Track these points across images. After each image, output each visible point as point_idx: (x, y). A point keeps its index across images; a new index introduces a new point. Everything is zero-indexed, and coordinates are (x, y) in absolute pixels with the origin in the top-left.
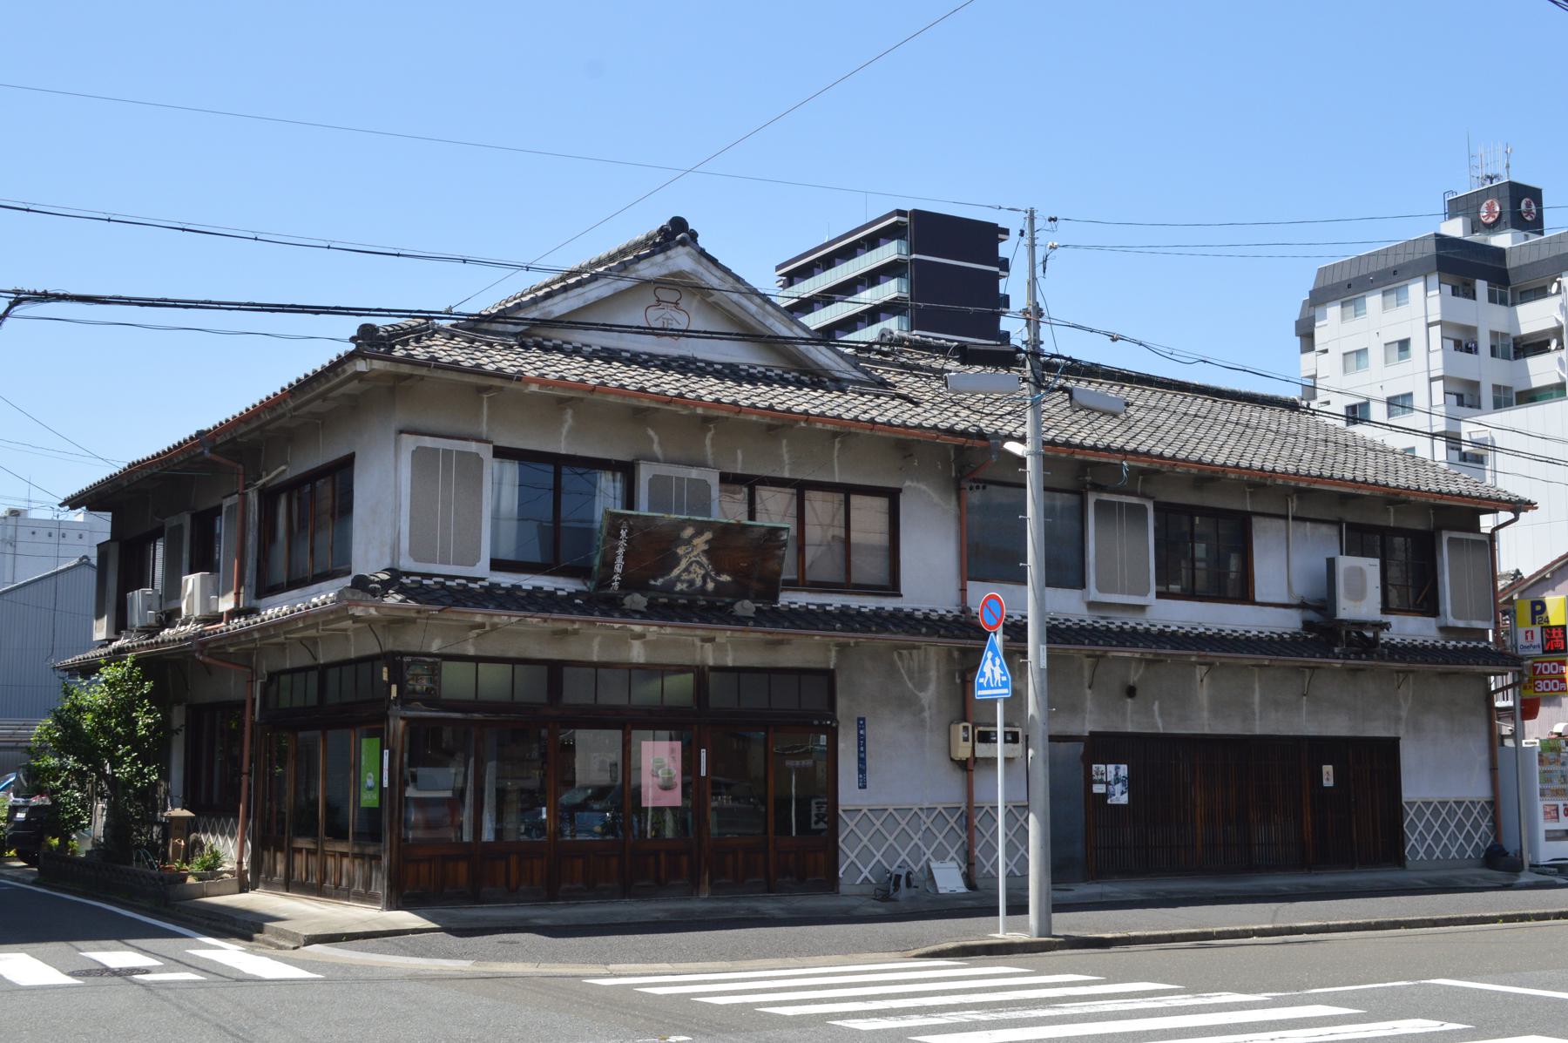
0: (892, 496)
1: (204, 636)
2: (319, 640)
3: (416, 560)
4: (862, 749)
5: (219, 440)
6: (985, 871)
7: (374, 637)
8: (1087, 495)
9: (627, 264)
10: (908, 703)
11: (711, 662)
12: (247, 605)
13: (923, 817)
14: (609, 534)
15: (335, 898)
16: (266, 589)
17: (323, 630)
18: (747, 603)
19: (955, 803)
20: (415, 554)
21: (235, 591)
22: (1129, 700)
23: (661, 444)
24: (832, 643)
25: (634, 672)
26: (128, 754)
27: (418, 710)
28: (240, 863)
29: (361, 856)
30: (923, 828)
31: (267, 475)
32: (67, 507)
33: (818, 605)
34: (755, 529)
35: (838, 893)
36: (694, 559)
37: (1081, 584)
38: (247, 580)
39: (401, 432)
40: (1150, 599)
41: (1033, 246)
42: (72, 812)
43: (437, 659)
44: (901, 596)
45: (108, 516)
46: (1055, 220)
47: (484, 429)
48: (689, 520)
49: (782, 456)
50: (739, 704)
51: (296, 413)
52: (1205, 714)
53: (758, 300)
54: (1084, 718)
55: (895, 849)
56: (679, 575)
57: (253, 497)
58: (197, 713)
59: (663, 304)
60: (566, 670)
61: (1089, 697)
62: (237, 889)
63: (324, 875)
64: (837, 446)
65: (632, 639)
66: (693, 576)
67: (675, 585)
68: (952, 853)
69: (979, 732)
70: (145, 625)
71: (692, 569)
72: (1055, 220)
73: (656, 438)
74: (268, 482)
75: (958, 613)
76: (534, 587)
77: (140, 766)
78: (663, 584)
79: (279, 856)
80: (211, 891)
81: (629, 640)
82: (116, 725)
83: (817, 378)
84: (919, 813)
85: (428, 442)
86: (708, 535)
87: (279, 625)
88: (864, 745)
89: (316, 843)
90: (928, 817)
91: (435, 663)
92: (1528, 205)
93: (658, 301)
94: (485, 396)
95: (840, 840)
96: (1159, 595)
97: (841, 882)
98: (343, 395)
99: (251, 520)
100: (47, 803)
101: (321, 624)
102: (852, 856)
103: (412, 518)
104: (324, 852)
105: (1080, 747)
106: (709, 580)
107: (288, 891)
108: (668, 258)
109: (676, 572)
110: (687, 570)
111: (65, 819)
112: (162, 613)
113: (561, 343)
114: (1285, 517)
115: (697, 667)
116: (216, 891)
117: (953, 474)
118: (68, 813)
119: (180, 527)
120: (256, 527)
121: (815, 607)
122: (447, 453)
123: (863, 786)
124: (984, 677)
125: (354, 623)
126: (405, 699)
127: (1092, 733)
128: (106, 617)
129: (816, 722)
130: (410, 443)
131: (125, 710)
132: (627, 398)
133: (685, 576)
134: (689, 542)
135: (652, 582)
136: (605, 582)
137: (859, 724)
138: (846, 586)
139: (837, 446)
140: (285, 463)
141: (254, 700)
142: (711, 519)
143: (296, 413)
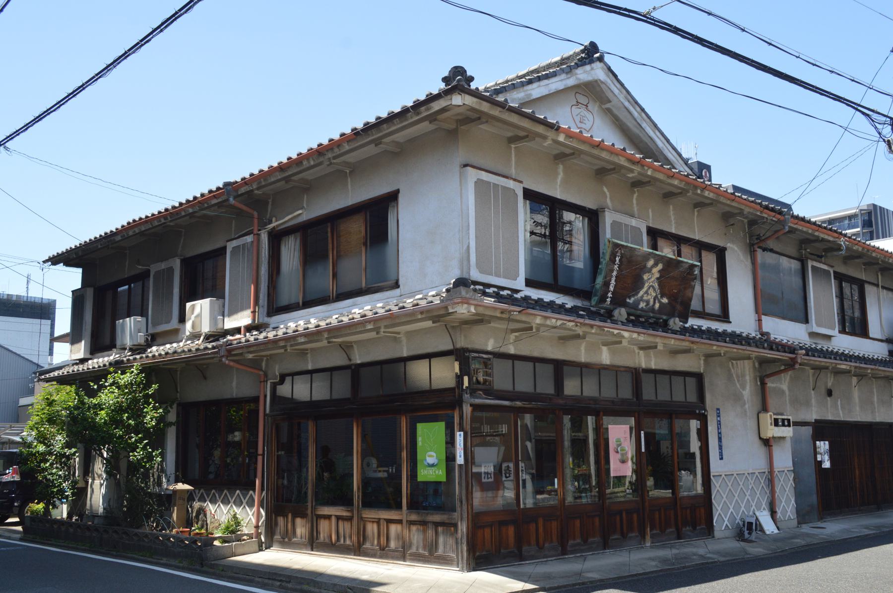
1: (231, 344)
2: (353, 344)
3: (481, 272)
5: (242, 190)
7: (449, 335)
8: (807, 262)
9: (572, 68)
10: (737, 398)
11: (644, 366)
12: (261, 321)
13: (750, 479)
15: (381, 557)
16: (276, 308)
17: (384, 332)
19: (762, 469)
21: (252, 309)
22: (828, 398)
23: (611, 199)
24: (701, 354)
25: (603, 372)
26: (140, 441)
27: (481, 398)
28: (257, 527)
29: (424, 523)
30: (750, 488)
31: (276, 221)
32: (50, 263)
33: (698, 326)
34: (684, 265)
35: (713, 537)
37: (807, 321)
38: (261, 302)
39: (466, 165)
40: (835, 332)
42: (59, 486)
43: (490, 356)
44: (731, 322)
45: (79, 271)
47: (513, 172)
48: (652, 253)
49: (670, 217)
50: (657, 398)
51: (335, 161)
52: (858, 408)
53: (638, 109)
54: (812, 410)
55: (727, 505)
56: (642, 296)
57: (264, 237)
58: (186, 409)
59: (580, 105)
61: (813, 395)
62: (257, 548)
63: (363, 537)
64: (696, 214)
65: (603, 345)
67: (639, 304)
68: (764, 506)
70: (136, 343)
73: (608, 194)
74: (278, 226)
77: (150, 450)
79: (299, 521)
80: (240, 550)
81: (601, 346)
82: (128, 418)
85: (485, 176)
87: (289, 339)
89: (352, 511)
90: (752, 480)
91: (489, 359)
92: (706, 173)
93: (577, 102)
94: (513, 146)
95: (713, 497)
96: (840, 332)
98: (393, 141)
99: (263, 255)
100: (16, 479)
101: (382, 327)
102: (719, 509)
103: (476, 237)
104: (361, 519)
106: (657, 301)
107: (312, 550)
108: (592, 69)
109: (641, 293)
110: (646, 292)
111: (53, 492)
112: (148, 336)
114: (877, 285)
115: (635, 369)
116: (240, 550)
117: (748, 241)
118: (55, 487)
119: (171, 270)
120: (267, 261)
121: (696, 327)
122: (496, 186)
123: (721, 459)
125: (433, 323)
126: (472, 391)
128: (83, 342)
130: (473, 175)
131: (135, 409)
132: (613, 156)
133: (645, 298)
134: (650, 271)
136: (603, 299)
139: (696, 214)
140: (302, 208)
141: (265, 396)
142: (664, 254)
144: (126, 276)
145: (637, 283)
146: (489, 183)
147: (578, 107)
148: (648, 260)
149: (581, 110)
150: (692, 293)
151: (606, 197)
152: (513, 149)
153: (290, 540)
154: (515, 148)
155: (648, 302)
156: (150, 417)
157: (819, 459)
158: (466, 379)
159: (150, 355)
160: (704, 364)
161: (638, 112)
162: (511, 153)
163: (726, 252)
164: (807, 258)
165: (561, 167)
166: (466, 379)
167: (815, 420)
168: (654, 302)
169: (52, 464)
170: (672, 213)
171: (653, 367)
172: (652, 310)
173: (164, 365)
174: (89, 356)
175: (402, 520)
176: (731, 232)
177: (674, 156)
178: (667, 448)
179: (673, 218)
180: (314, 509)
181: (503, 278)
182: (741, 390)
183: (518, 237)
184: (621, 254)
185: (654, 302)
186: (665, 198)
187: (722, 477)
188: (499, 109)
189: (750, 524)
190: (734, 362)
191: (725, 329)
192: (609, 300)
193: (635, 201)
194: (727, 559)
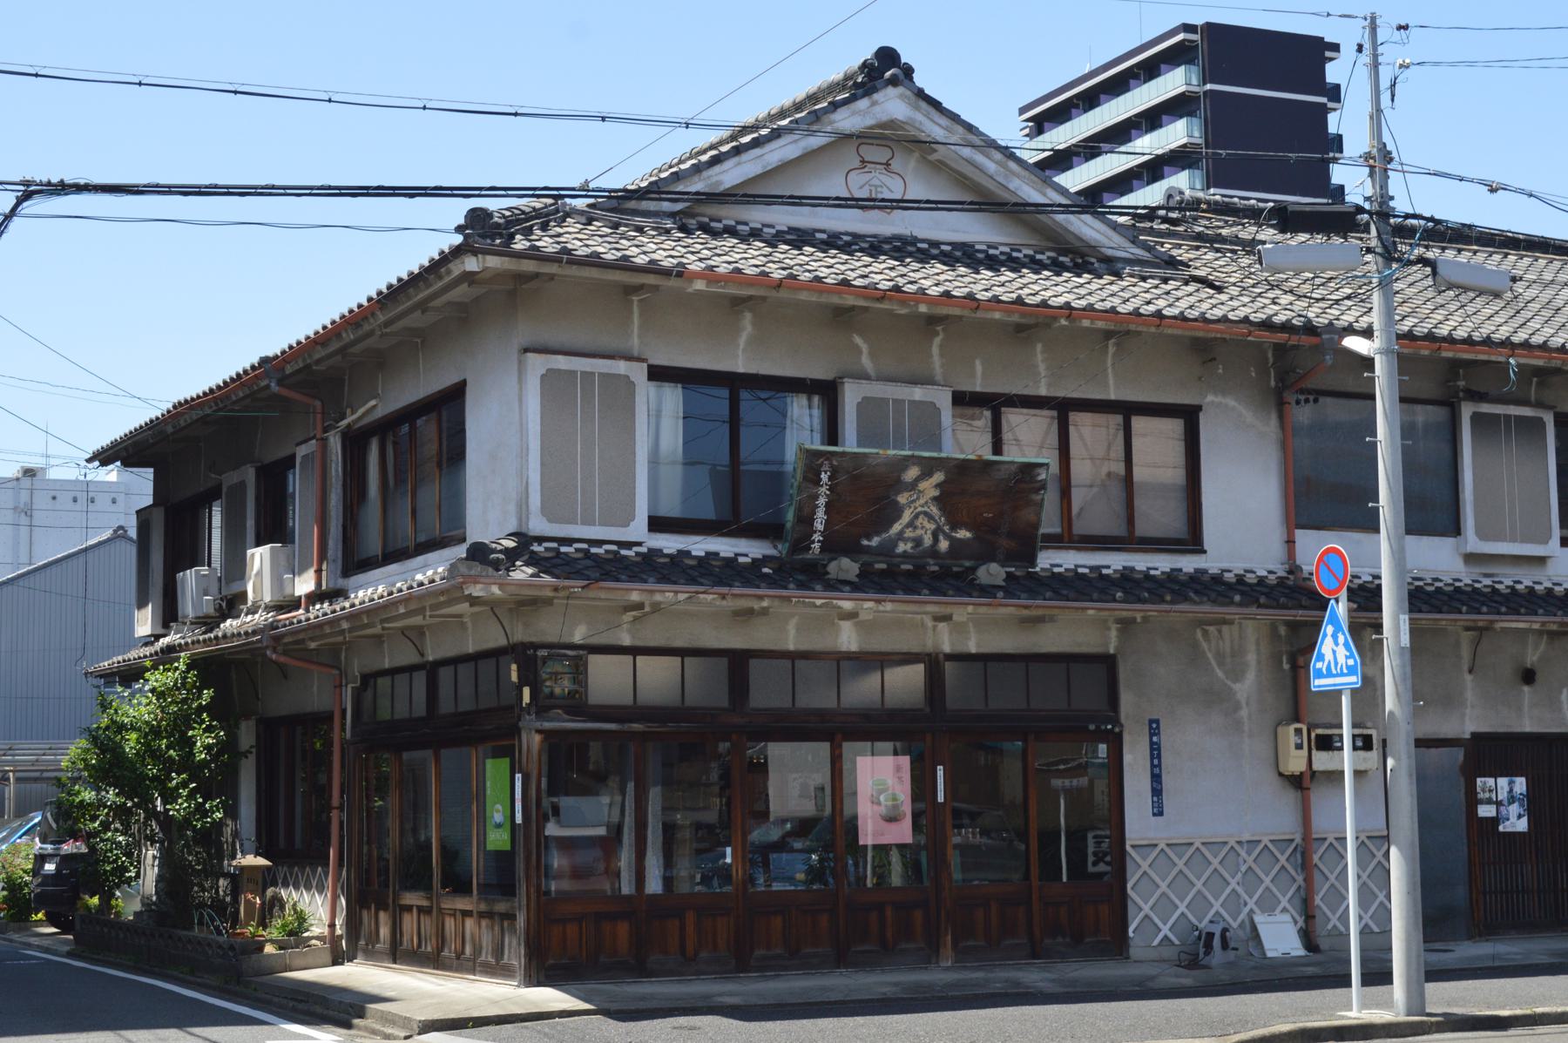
0: (1189, 416)
3: (550, 521)
4: (1156, 762)
6: (1330, 927)
10: (1217, 699)
11: (947, 648)
13: (1243, 854)
14: (805, 478)
15: (457, 970)
16: (356, 563)
17: (430, 617)
18: (994, 567)
19: (1284, 834)
20: (548, 512)
22: (1526, 689)
26: (184, 785)
27: (559, 720)
30: (1243, 869)
31: (352, 414)
35: (1128, 958)
36: (920, 509)
37: (1455, 529)
38: (330, 553)
39: (526, 350)
41: (1375, 65)
42: (115, 861)
43: (581, 652)
44: (1205, 552)
46: (1405, 27)
47: (635, 344)
50: (987, 705)
51: (388, 330)
53: (998, 156)
56: (901, 532)
57: (335, 443)
58: (270, 729)
59: (869, 165)
60: (753, 663)
64: (1111, 350)
66: (919, 532)
67: (896, 546)
68: (1284, 902)
69: (1317, 736)
70: (201, 615)
71: (918, 523)
72: (1405, 27)
73: (864, 347)
75: (1284, 574)
76: (707, 553)
77: (200, 800)
78: (881, 545)
81: (836, 621)
82: (168, 747)
83: (1082, 258)
84: (1237, 847)
85: (562, 362)
86: (939, 477)
87: (374, 611)
88: (1159, 757)
89: (430, 899)
93: (863, 161)
94: (635, 298)
95: (1129, 886)
97: (1132, 943)
98: (449, 303)
99: (333, 473)
102: (1146, 909)
104: (440, 910)
105: (1459, 754)
106: (941, 538)
107: (395, 963)
108: (874, 104)
109: (897, 528)
110: (911, 524)
111: (105, 871)
113: (733, 223)
115: (929, 655)
116: (298, 962)
117: (1273, 383)
118: (109, 863)
120: (340, 483)
121: (1086, 571)
122: (588, 376)
124: (1323, 660)
125: (471, 605)
127: (1476, 736)
129: (1092, 727)
130: (538, 364)
131: (178, 727)
133: (909, 533)
134: (913, 486)
135: (865, 542)
136: (802, 544)
137: (1151, 728)
138: (1128, 541)
139: (1111, 350)
141: (344, 712)
142: (943, 455)
143: (388, 330)
144: (202, 489)
145: (886, 513)
146: (573, 373)
147: (866, 170)
148: (905, 468)
149: (871, 175)
150: (1039, 514)
151: (860, 352)
152: (635, 303)
153: (373, 947)
154: (640, 301)
155: (918, 542)
156: (203, 740)
157: (1486, 811)
158: (526, 691)
159: (220, 634)
160: (1118, 637)
161: (996, 163)
162: (631, 312)
163: (1201, 415)
164: (1459, 402)
165: (748, 316)
166: (526, 691)
167: (1473, 734)
168: (936, 540)
169: (106, 826)
170: (1040, 357)
171: (973, 650)
172: (933, 552)
173: (230, 654)
174: (160, 631)
175: (472, 911)
176: (1220, 371)
177: (1098, 231)
178: (1103, 792)
179: (1042, 368)
180: (396, 897)
181: (600, 525)
182: (1229, 683)
183: (634, 453)
184: (832, 466)
185: (936, 540)
186: (1018, 332)
187: (1159, 848)
188: (556, 265)
189: (1210, 935)
190: (1211, 629)
191: (1178, 566)
192: (816, 546)
193: (935, 350)
194: (1066, 990)
